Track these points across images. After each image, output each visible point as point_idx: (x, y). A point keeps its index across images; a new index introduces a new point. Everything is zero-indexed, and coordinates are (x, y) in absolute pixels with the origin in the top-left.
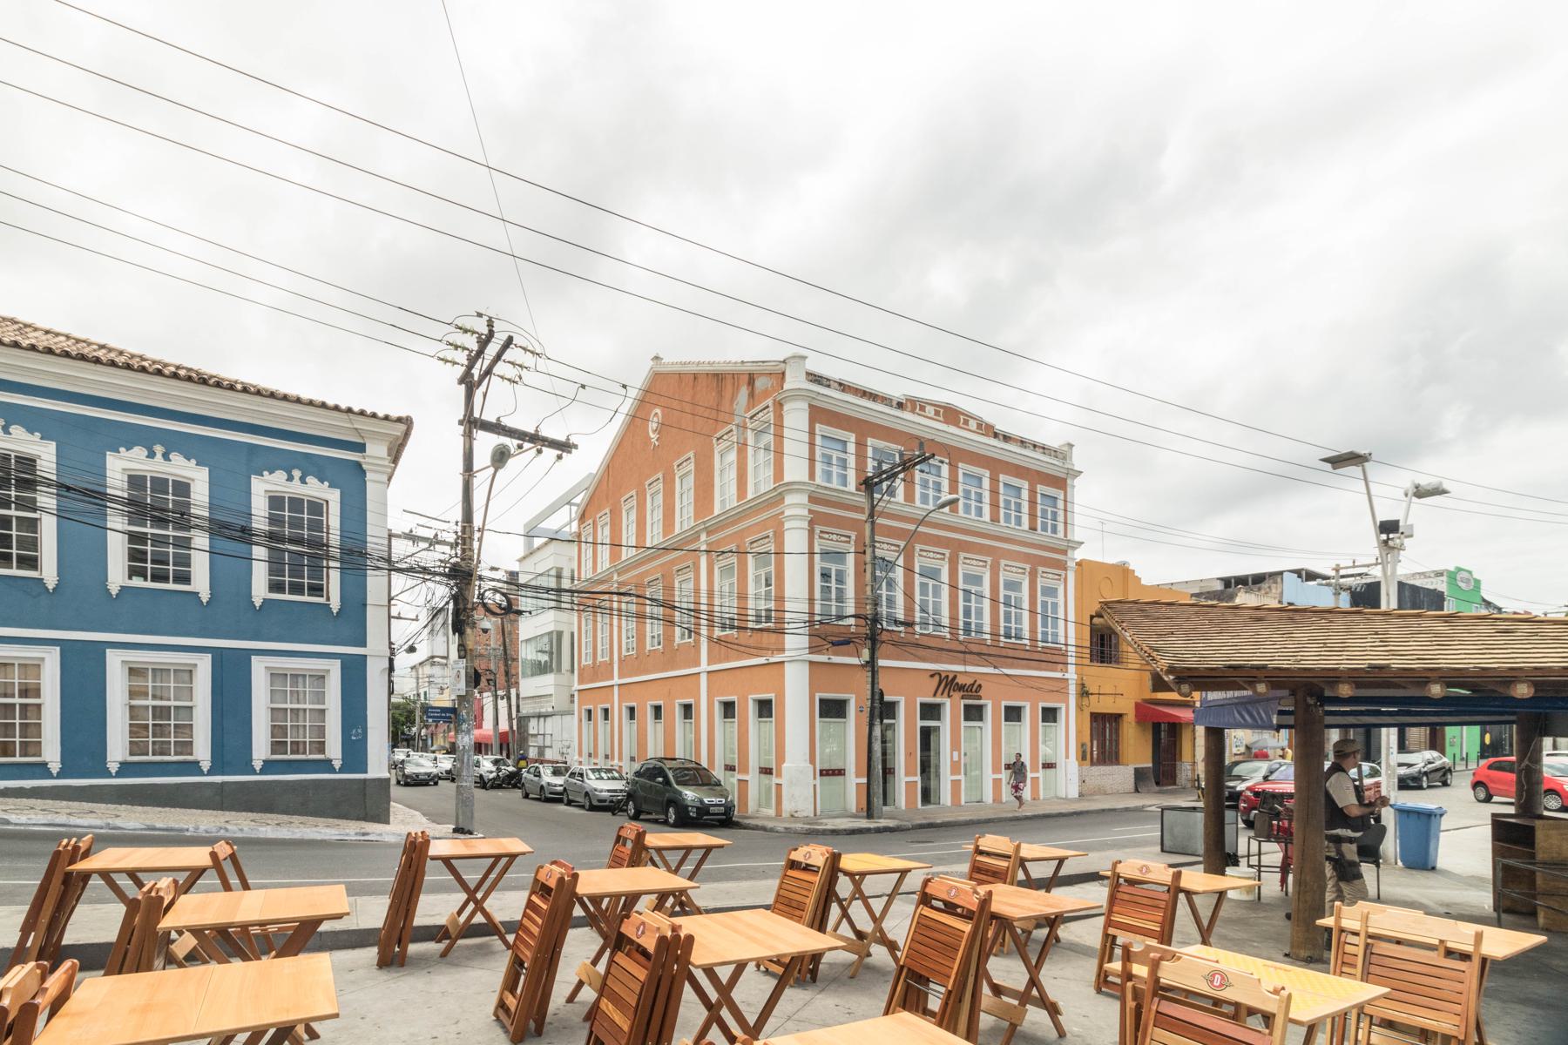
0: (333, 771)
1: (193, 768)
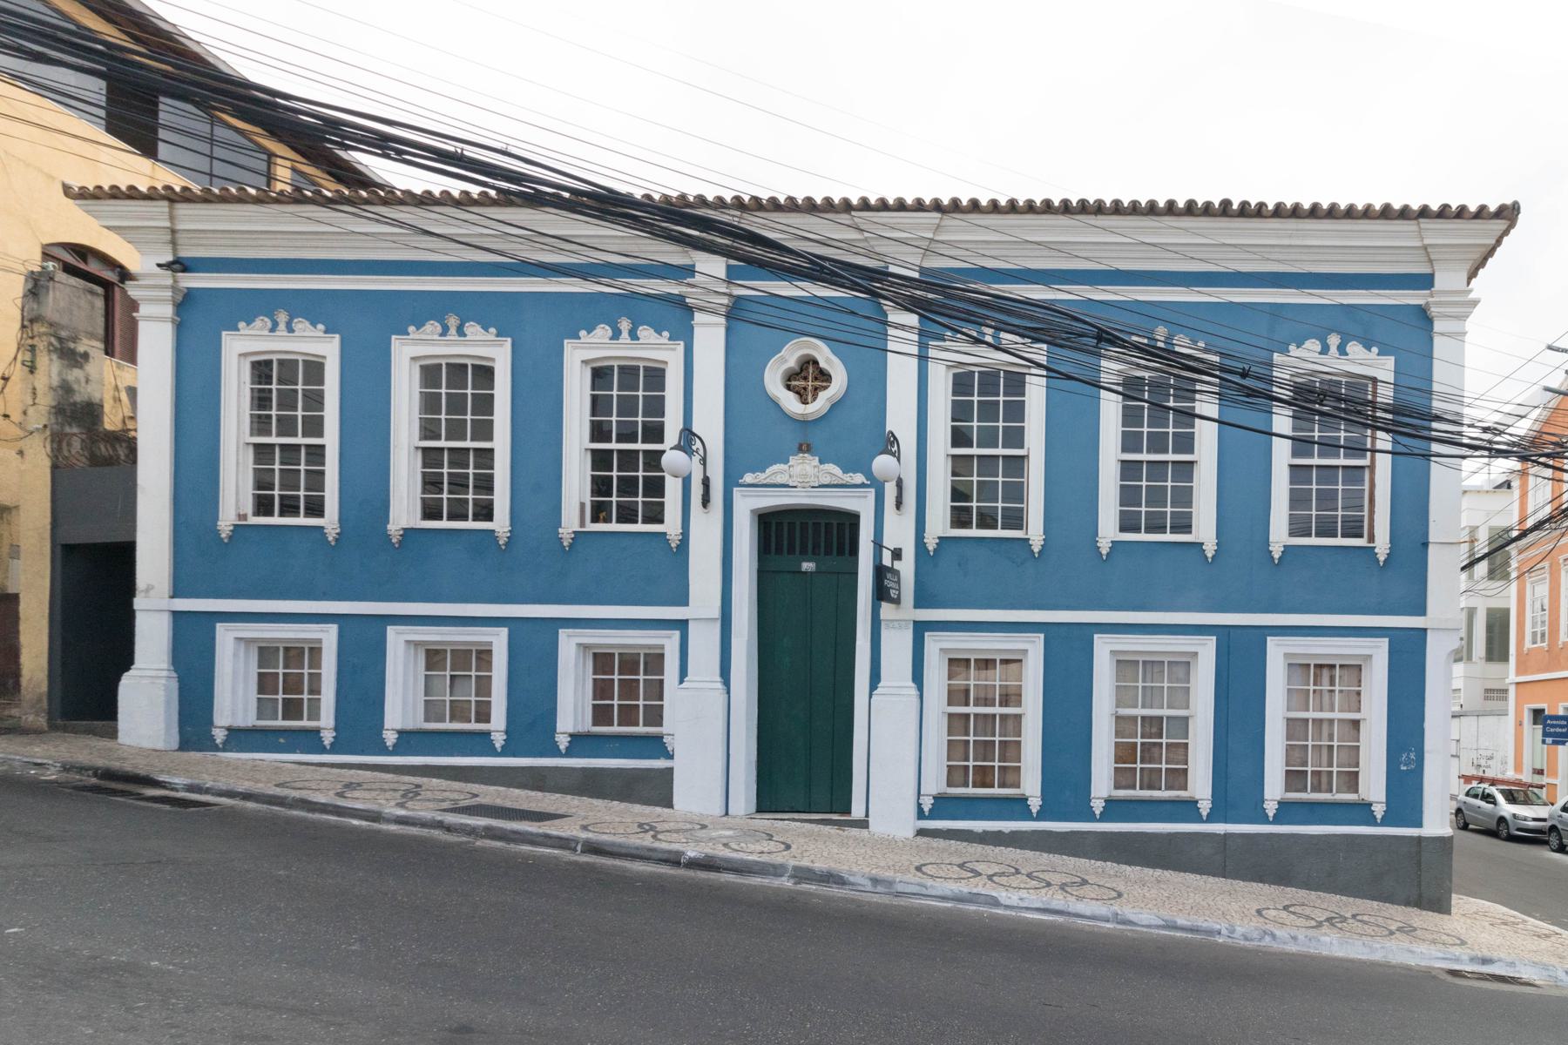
0: (1371, 820)
1: (1187, 809)
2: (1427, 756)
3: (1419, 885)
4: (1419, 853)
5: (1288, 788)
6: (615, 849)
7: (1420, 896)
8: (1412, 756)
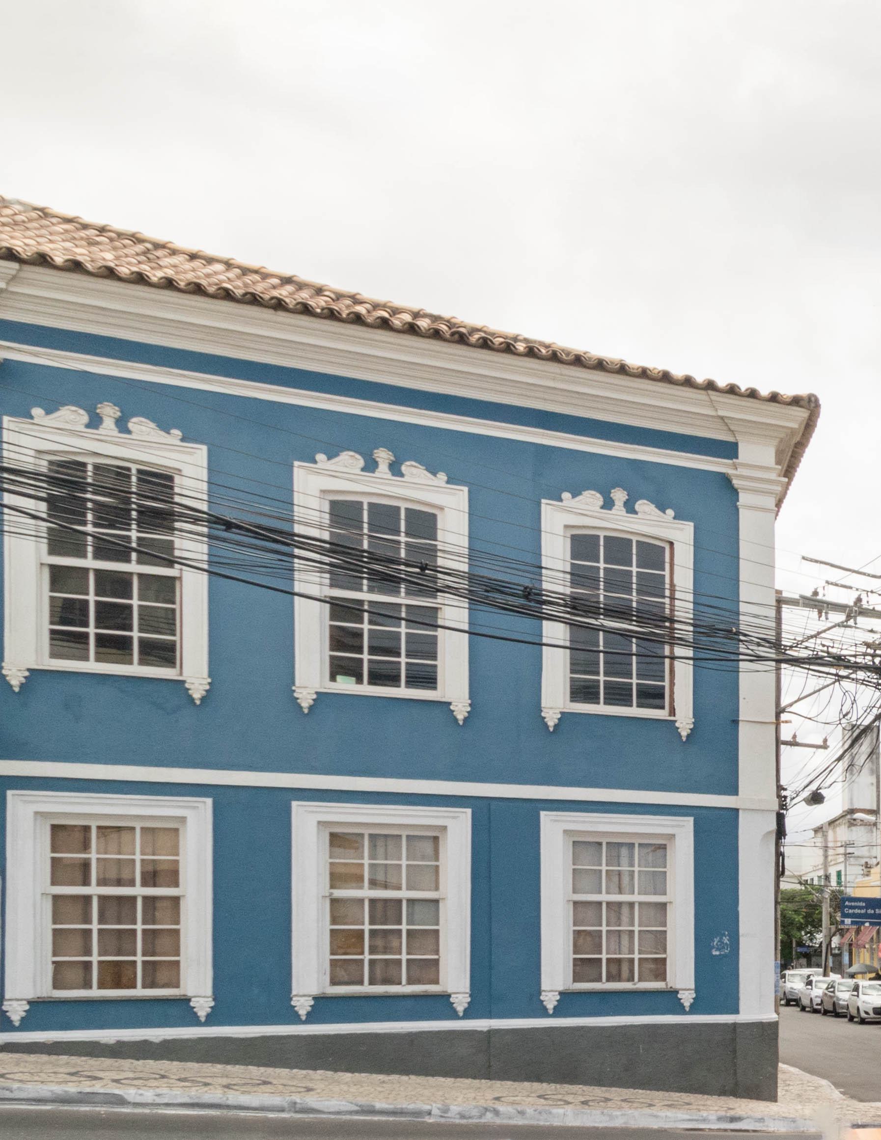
0: (679, 1009)
1: (440, 1005)
2: (742, 940)
3: (735, 1073)
4: (734, 1040)
5: (577, 978)
6: (425, 627)
7: (736, 1084)
8: (726, 940)
